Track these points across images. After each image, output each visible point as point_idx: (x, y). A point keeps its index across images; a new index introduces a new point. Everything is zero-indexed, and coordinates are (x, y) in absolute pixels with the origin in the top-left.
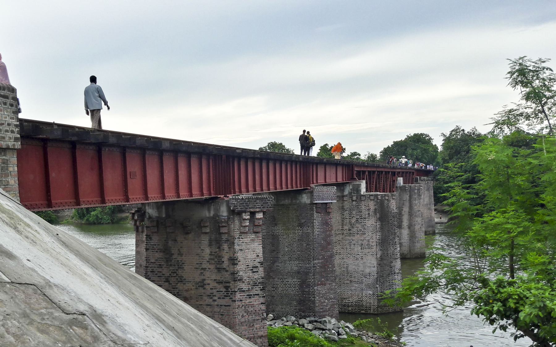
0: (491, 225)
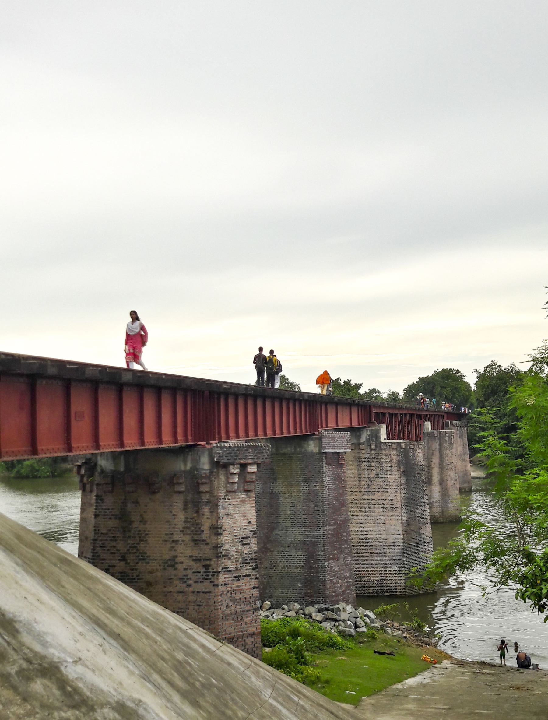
0: (534, 484)
